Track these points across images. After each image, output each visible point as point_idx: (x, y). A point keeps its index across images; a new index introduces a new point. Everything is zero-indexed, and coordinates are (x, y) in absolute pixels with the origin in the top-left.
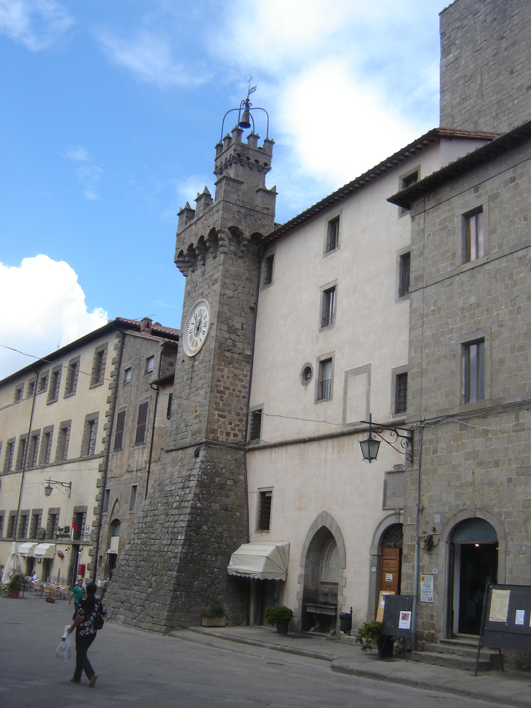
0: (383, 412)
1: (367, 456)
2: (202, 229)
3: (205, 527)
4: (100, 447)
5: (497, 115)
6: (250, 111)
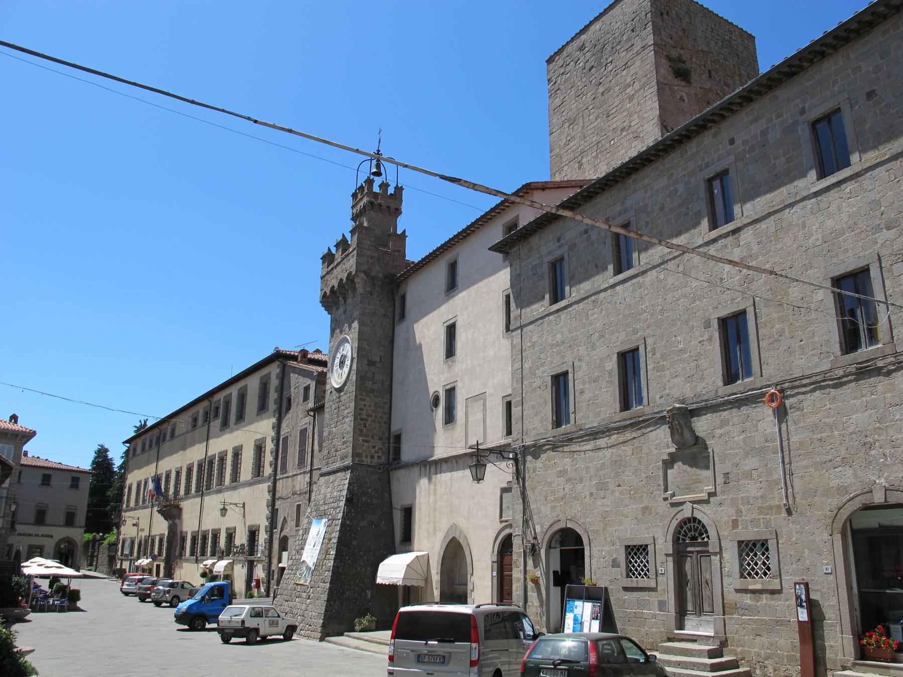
0: (495, 437)
3: (354, 543)
4: (268, 470)
5: (597, 154)
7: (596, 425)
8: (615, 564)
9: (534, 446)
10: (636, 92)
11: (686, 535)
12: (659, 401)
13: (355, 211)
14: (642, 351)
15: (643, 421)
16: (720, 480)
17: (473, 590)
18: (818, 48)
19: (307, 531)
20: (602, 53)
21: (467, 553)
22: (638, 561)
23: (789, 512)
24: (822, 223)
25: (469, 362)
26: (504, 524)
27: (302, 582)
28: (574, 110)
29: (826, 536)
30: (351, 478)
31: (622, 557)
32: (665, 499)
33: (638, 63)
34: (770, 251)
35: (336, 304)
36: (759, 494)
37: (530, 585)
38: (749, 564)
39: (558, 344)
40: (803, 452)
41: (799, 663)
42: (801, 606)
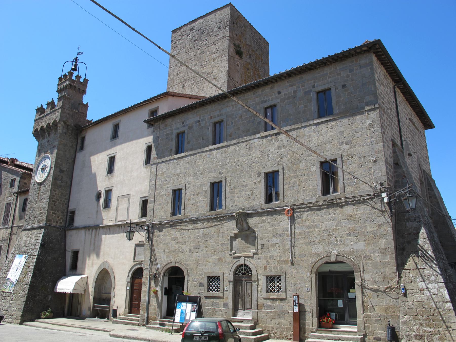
1: (128, 238)
2: (48, 120)
5: (193, 83)
6: (78, 63)
7: (196, 216)
8: (201, 285)
9: (159, 224)
10: (217, 57)
11: (240, 272)
12: (231, 208)
13: (59, 87)
14: (224, 183)
15: (222, 217)
16: (260, 247)
17: (114, 297)
18: (324, 61)
19: (12, 261)
20: (203, 34)
21: (112, 277)
22: (213, 284)
23: (292, 263)
24: (318, 137)
25: (122, 177)
26: (136, 263)
27: (7, 291)
28: (184, 59)
29: (308, 275)
30: (44, 233)
31: (205, 281)
32: (231, 255)
33: (220, 44)
34: (293, 145)
35: (42, 136)
36: (278, 255)
37: (152, 294)
38: (271, 287)
39: (177, 175)
40: (301, 237)
41: (292, 330)
42: (296, 305)
